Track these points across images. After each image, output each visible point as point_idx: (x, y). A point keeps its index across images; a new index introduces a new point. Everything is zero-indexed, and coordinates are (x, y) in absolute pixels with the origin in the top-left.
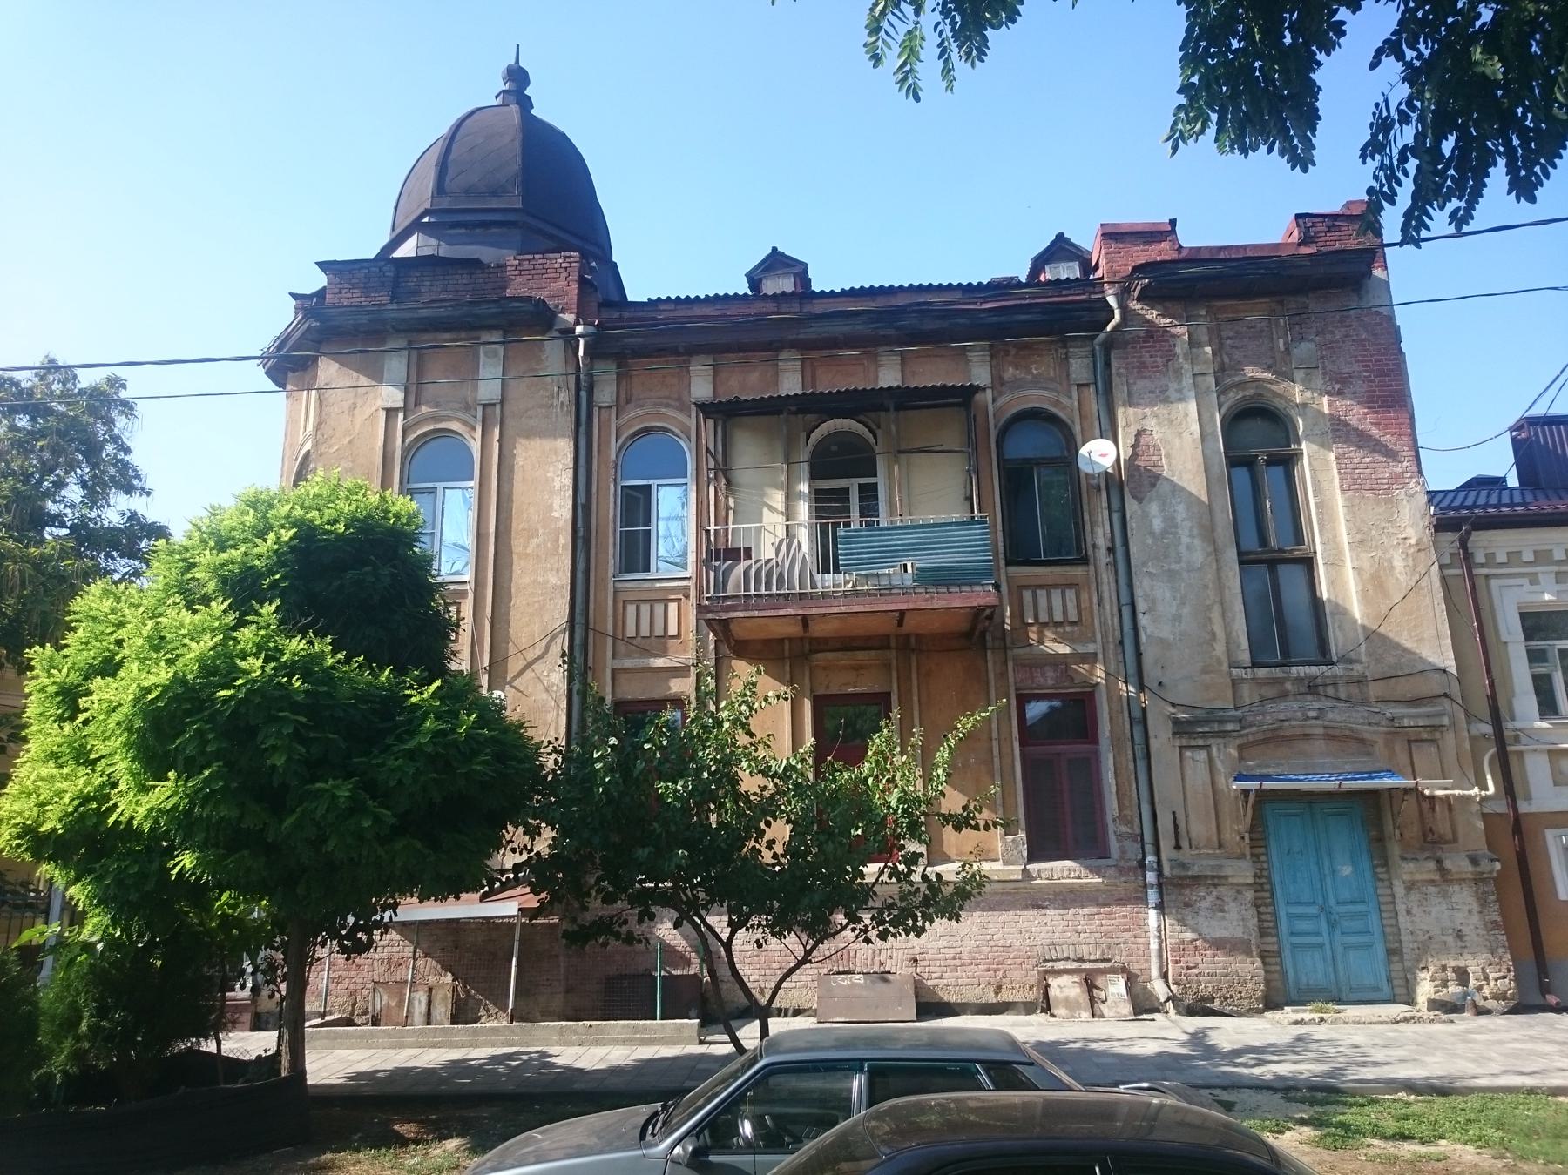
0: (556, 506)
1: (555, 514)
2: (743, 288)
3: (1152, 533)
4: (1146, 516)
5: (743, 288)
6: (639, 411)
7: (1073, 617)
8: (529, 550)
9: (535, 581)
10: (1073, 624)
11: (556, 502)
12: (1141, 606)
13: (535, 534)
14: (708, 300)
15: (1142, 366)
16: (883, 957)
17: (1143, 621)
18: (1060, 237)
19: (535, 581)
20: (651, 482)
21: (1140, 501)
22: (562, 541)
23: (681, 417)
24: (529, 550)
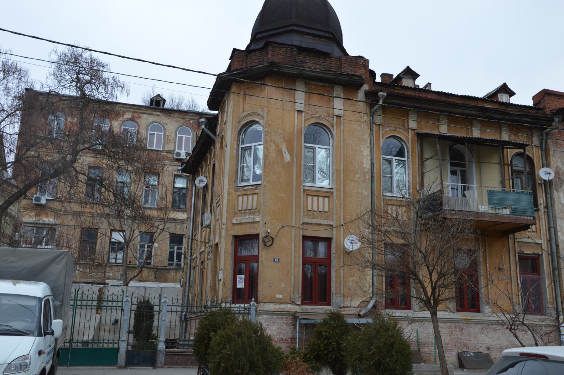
0: (365, 163)
1: (365, 166)
2: (530, 103)
3: (561, 203)
4: (559, 197)
5: (530, 103)
6: (390, 128)
7: (326, 210)
8: (355, 179)
9: (358, 192)
10: (534, 232)
11: (365, 161)
12: (559, 229)
13: (357, 173)
14: (462, 96)
15: (557, 143)
16: (478, 347)
17: (559, 234)
18: (505, 85)
19: (358, 192)
20: (315, 146)
21: (557, 191)
22: (367, 177)
23: (406, 133)
24: (355, 179)
